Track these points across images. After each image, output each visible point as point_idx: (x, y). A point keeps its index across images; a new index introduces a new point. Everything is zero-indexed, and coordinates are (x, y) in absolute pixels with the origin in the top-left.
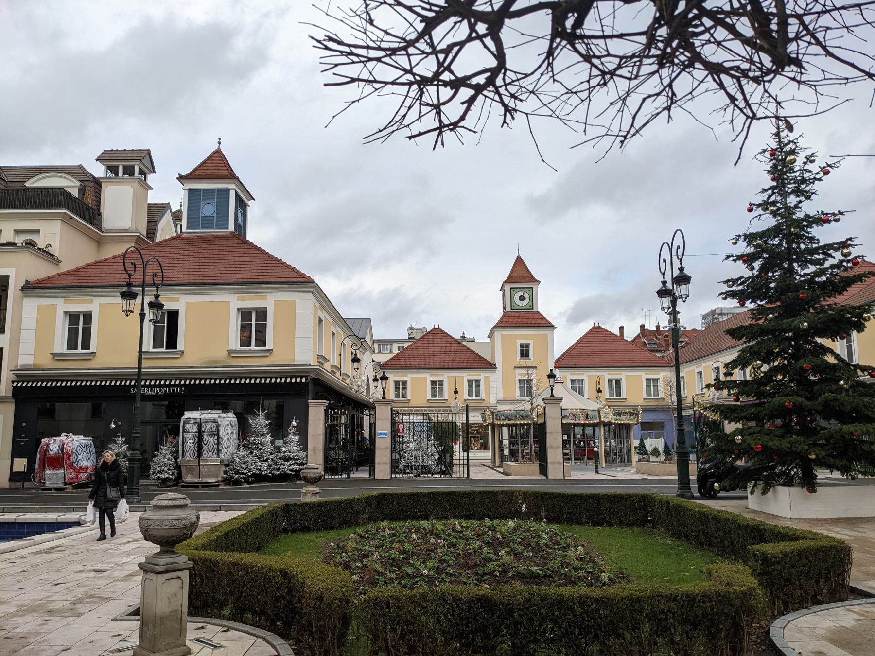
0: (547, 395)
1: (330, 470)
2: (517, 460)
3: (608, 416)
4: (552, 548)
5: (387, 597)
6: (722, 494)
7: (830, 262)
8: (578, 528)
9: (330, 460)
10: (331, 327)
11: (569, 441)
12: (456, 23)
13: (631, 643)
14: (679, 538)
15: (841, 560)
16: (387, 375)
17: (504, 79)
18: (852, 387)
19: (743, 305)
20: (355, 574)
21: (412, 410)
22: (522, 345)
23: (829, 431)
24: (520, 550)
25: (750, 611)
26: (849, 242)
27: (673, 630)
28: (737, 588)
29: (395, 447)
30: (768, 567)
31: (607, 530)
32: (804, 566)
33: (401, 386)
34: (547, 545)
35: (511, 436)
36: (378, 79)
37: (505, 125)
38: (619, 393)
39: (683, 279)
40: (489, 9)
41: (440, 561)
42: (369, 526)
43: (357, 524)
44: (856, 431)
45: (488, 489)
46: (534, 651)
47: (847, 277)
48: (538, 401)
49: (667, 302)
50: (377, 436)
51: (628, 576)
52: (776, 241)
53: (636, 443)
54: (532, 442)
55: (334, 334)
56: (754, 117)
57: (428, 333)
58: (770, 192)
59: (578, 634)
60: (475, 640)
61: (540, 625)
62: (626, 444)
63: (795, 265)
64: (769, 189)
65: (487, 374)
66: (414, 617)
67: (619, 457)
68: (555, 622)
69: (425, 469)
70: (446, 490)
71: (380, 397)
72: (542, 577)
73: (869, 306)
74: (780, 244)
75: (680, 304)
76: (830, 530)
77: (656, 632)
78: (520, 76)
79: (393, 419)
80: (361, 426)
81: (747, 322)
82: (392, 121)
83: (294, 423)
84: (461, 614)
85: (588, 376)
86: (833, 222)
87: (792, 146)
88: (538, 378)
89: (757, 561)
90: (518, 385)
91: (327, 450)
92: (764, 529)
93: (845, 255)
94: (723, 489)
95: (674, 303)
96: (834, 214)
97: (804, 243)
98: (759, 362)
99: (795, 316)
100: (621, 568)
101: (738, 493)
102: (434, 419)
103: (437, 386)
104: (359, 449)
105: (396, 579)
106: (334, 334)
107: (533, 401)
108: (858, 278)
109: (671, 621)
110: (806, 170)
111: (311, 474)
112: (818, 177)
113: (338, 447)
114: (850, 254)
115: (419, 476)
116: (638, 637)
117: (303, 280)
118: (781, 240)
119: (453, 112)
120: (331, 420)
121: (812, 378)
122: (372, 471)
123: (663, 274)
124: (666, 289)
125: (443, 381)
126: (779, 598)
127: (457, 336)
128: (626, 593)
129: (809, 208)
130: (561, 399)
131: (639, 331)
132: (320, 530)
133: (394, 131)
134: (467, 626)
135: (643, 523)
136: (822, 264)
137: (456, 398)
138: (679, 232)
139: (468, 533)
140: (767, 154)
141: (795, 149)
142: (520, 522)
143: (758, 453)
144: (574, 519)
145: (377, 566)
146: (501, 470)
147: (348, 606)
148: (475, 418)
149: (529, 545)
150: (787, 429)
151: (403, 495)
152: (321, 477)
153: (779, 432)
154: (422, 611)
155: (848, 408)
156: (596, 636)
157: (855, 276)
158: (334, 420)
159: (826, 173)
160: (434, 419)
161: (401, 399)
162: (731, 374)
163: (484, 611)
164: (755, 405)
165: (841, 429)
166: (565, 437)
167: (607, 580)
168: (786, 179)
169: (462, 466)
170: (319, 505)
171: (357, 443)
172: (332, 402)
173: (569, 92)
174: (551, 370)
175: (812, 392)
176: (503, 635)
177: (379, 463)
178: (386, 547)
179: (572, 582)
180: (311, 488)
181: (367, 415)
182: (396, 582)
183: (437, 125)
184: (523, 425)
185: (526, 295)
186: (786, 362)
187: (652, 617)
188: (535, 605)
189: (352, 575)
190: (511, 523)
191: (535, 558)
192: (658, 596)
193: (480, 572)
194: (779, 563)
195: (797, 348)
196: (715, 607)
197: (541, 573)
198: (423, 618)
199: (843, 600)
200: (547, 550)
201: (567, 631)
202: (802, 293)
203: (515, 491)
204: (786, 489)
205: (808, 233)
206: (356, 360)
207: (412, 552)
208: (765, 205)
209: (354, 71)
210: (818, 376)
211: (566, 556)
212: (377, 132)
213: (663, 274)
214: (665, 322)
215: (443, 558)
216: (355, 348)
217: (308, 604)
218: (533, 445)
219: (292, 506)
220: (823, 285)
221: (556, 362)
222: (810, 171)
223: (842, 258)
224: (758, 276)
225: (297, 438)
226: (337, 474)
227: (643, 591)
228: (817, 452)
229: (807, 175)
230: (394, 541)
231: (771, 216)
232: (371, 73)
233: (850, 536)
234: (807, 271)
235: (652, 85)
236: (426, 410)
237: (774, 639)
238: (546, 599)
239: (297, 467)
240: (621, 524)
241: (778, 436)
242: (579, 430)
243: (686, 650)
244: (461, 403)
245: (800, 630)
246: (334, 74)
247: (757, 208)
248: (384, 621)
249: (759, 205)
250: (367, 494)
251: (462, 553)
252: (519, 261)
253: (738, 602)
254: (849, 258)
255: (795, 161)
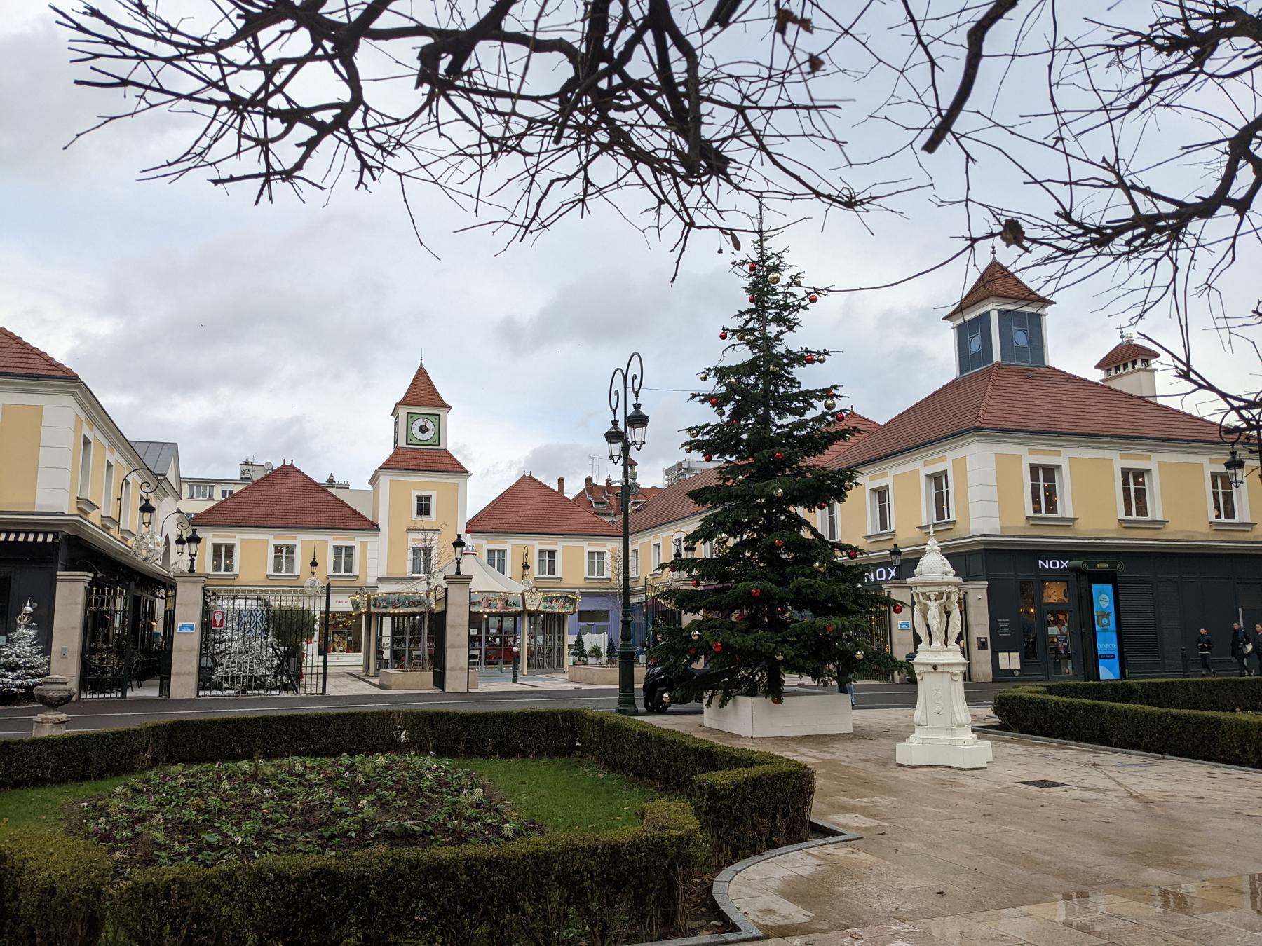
0: (451, 571)
1: (91, 684)
2: (402, 667)
3: (535, 603)
4: (437, 793)
5: (166, 882)
6: (673, 708)
7: (810, 414)
8: (478, 763)
9: (91, 670)
10: (104, 452)
11: (480, 638)
12: (283, 33)
13: (533, 918)
14: (614, 770)
15: (802, 790)
16: (199, 534)
17: (364, 121)
18: (828, 569)
19: (709, 460)
20: (119, 849)
21: (238, 591)
22: (420, 498)
23: (801, 625)
24: (390, 798)
25: (687, 861)
26: (834, 391)
27: (589, 897)
28: (673, 832)
29: (206, 649)
30: (715, 802)
31: (519, 763)
32: (758, 799)
33: (223, 553)
34: (431, 789)
35: (395, 631)
36: (165, 88)
37: (361, 186)
38: (552, 571)
39: (638, 420)
40: (345, 20)
41: (264, 822)
42: (150, 774)
43: (132, 771)
44: (830, 625)
45: (352, 711)
46: (396, 943)
47: (828, 433)
48: (439, 580)
49: (617, 448)
50: (177, 630)
51: (540, 827)
52: (751, 380)
53: (571, 639)
54: (426, 639)
55: (109, 466)
56: (691, 224)
57: (274, 472)
58: (747, 316)
59: (461, 913)
60: (307, 935)
61: (407, 905)
62: (557, 642)
63: (772, 412)
64: (747, 312)
65: (364, 539)
66: (210, 909)
67: (546, 660)
68: (428, 898)
69: (256, 682)
70: (285, 714)
71: (186, 569)
72: (419, 836)
73: (852, 472)
74: (756, 385)
75: (633, 451)
76: (796, 752)
77: (568, 898)
78: (388, 121)
79: (205, 604)
80: (151, 615)
81: (713, 483)
82: (188, 153)
83: (28, 609)
84: (286, 898)
85: (511, 545)
86: (817, 363)
87: (775, 260)
88: (441, 546)
89: (703, 795)
90: (411, 556)
91: (87, 652)
92: (716, 753)
93: (828, 407)
94: (674, 701)
95: (625, 450)
96: (818, 353)
97: (783, 386)
98: (724, 535)
99: (768, 479)
100: (533, 815)
101: (692, 705)
102: (275, 604)
103: (283, 553)
104: (146, 650)
105: (189, 854)
106: (109, 466)
107: (431, 580)
108: (842, 435)
109: (588, 883)
110: (789, 293)
111: (53, 692)
112: (803, 303)
113: (108, 648)
114: (834, 406)
115: (244, 692)
116: (542, 910)
117: (60, 373)
118: (757, 379)
119: (286, 153)
120: (108, 605)
121: (784, 557)
122: (165, 686)
123: (615, 411)
124: (617, 432)
125: (294, 546)
126: (727, 843)
127: (321, 479)
128: (530, 849)
129: (792, 342)
130: (471, 578)
131: (584, 486)
132: (65, 782)
133: (190, 169)
134: (295, 916)
135: (568, 750)
136: (802, 415)
137: (313, 573)
138: (636, 356)
139: (312, 776)
140: (747, 267)
141: (778, 265)
142: (396, 758)
143: (717, 653)
144: (474, 750)
145: (158, 835)
146: (377, 681)
147: (99, 899)
148: (341, 604)
149: (405, 789)
150: (753, 623)
151: (213, 722)
152: (70, 697)
153: (742, 626)
154: (224, 899)
155: (823, 597)
156: (486, 912)
157: (838, 432)
158: (102, 605)
159: (813, 300)
160: (275, 604)
161: (222, 572)
162: (693, 549)
163: (322, 891)
164: (717, 591)
165: (814, 623)
166: (474, 632)
167: (510, 833)
168: (767, 302)
169: (314, 676)
170: (65, 741)
171: (143, 642)
172: (100, 575)
173: (460, 151)
174: (459, 536)
175: (782, 575)
176: (351, 925)
177: (178, 674)
178: (177, 805)
179: (460, 838)
180: (51, 715)
181: (162, 598)
182: (188, 858)
183: (264, 170)
184: (414, 615)
185: (430, 425)
186: (755, 536)
187: (564, 879)
188: (400, 876)
189: (112, 850)
190: (381, 760)
191: (411, 809)
192: (572, 850)
193: (326, 834)
194: (728, 796)
195: (769, 518)
196: (644, 859)
197: (417, 829)
198: (225, 910)
199: (803, 841)
200: (431, 795)
201: (444, 909)
202: (779, 452)
203: (392, 712)
204: (749, 699)
205: (789, 373)
206: (147, 508)
207: (220, 810)
208: (742, 332)
209: (123, 68)
210: (792, 555)
211: (456, 802)
212: (163, 166)
213: (615, 411)
214: (617, 476)
215: (270, 816)
216: (147, 490)
217: (28, 901)
218: (427, 644)
219: (15, 744)
220: (802, 441)
221: (469, 524)
222: (794, 296)
223: (825, 410)
224: (728, 424)
225: (33, 633)
226: (104, 692)
227: (553, 845)
228: (786, 651)
229: (790, 300)
230: (191, 794)
231: (748, 348)
232: (154, 77)
233: (818, 759)
234: (784, 422)
235: (570, 162)
236: (261, 591)
237: (716, 896)
238: (418, 866)
239: (30, 681)
240: (540, 753)
241: (741, 631)
242: (494, 622)
243: (605, 921)
244: (320, 581)
245: (749, 883)
246: (92, 68)
247: (733, 335)
248: (160, 918)
249: (735, 332)
250: (152, 722)
251: (300, 807)
252: (422, 375)
253: (672, 851)
254: (834, 411)
255: (778, 280)
